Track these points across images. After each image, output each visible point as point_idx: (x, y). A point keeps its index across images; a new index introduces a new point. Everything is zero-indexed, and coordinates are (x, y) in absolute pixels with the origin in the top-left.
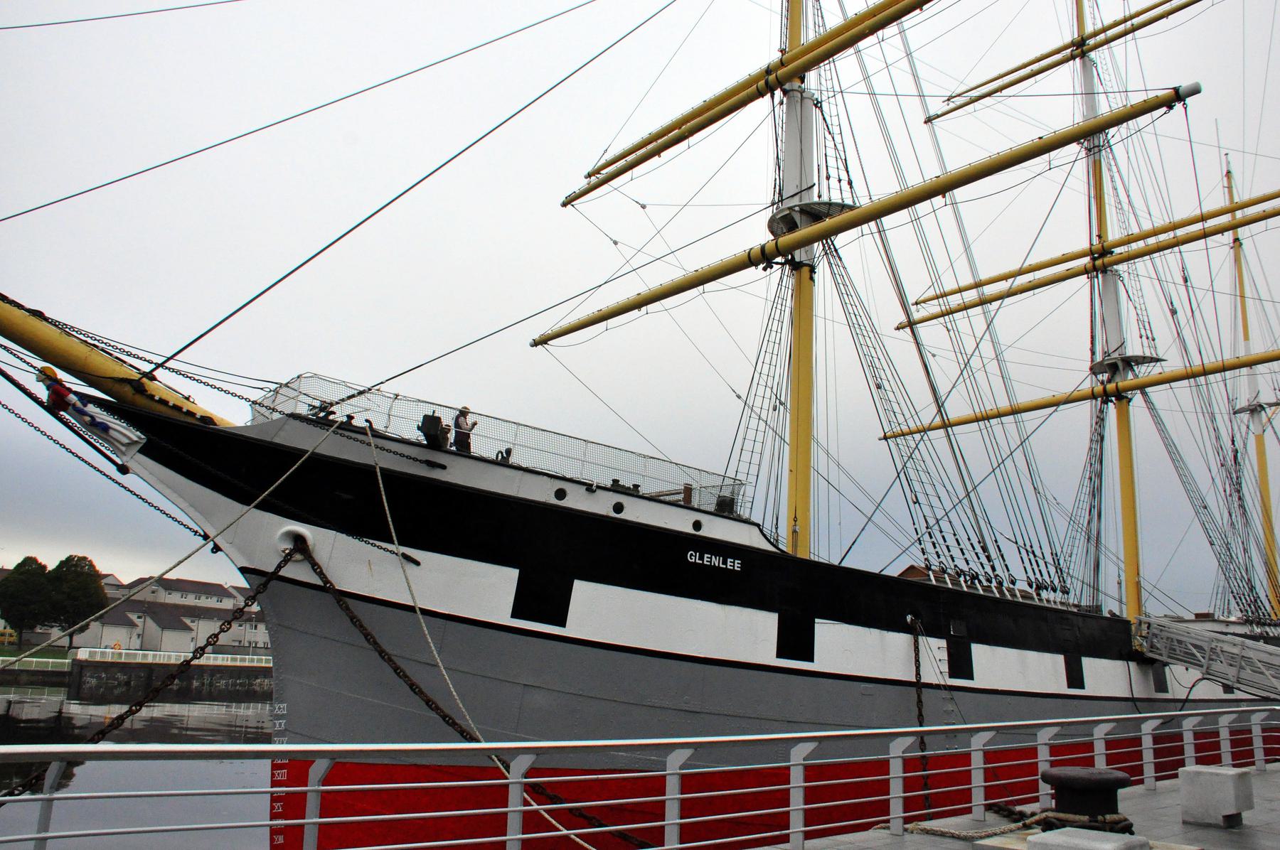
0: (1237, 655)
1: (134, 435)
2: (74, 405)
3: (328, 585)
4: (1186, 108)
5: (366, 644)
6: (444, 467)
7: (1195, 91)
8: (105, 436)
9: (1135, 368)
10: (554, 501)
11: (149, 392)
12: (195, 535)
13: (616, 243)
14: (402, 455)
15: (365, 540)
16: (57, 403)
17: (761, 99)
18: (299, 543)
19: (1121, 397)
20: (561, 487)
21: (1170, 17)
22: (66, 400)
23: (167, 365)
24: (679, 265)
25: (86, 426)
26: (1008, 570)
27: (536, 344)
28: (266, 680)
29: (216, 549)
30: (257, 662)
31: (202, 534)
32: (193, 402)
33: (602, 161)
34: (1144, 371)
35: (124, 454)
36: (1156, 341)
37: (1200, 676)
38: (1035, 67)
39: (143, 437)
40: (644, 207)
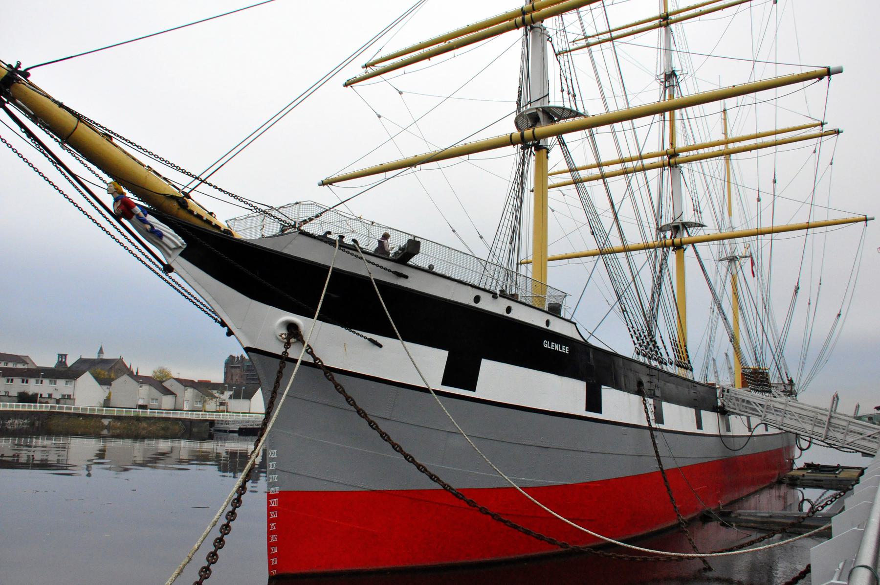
0: (782, 409)
1: (180, 241)
2: (138, 216)
3: (317, 362)
4: (829, 81)
5: (348, 406)
6: (406, 277)
7: (839, 71)
8: (158, 242)
9: (688, 229)
10: (473, 304)
11: (189, 208)
12: (216, 322)
13: (379, 116)
14: (381, 267)
15: (353, 330)
16: (124, 211)
17: (516, 30)
18: (292, 328)
19: (679, 247)
20: (477, 294)
21: (724, 10)
22: (132, 210)
23: (184, 187)
24: (421, 136)
25: (146, 233)
26: (668, 356)
27: (323, 184)
28: (16, 421)
29: (230, 333)
30: (74, 410)
31: (220, 321)
32: (215, 218)
33: (378, 57)
34: (696, 233)
35: (170, 256)
36: (702, 214)
37: (759, 422)
38: (635, 28)
39: (185, 243)
40: (401, 93)
